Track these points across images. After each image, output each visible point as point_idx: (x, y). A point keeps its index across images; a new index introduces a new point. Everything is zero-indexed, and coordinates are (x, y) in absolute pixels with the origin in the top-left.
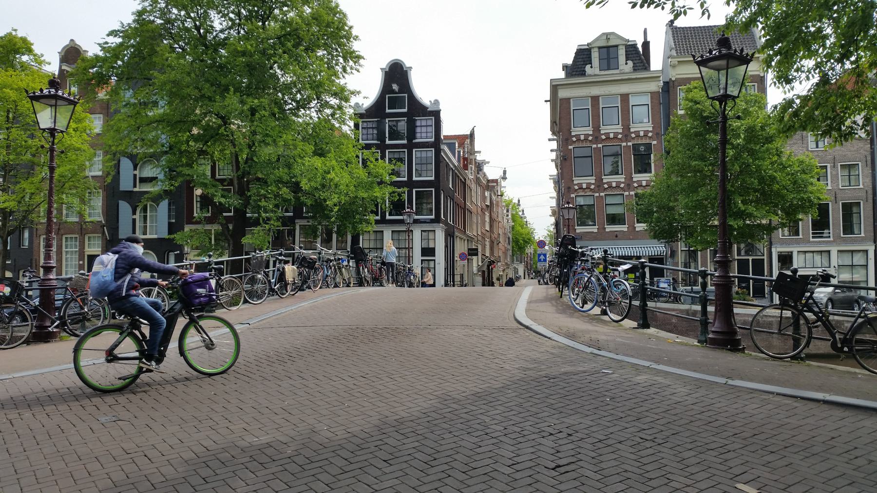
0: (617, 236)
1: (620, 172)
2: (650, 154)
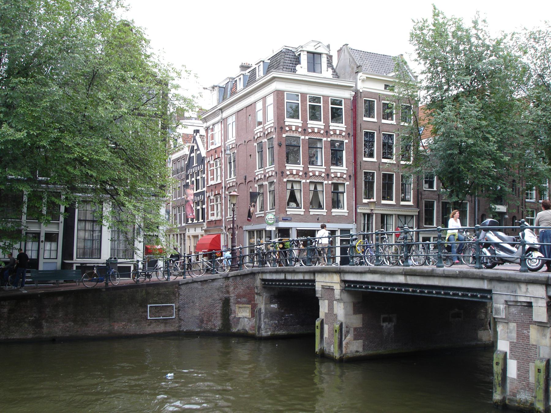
0: (318, 219)
1: (319, 163)
2: (342, 151)
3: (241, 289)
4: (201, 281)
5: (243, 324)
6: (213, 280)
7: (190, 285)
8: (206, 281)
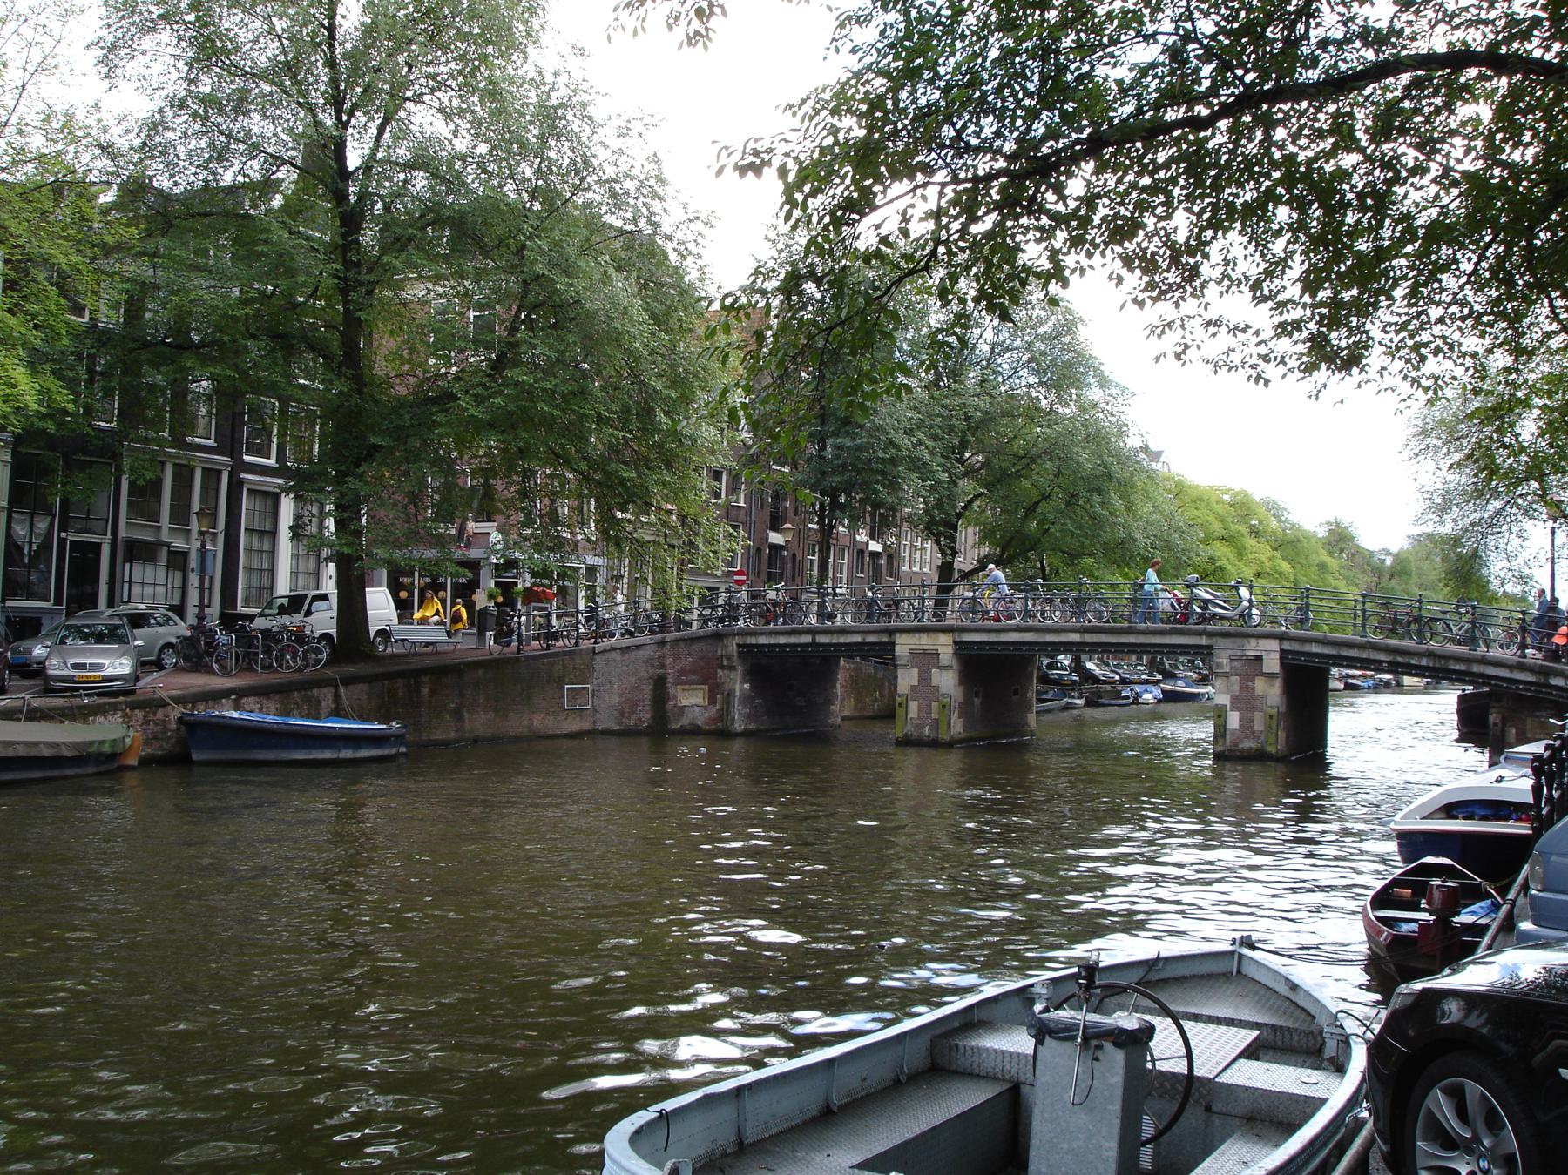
3: (687, 661)
4: (621, 649)
5: (690, 716)
6: (638, 647)
7: (607, 655)
8: (628, 647)
